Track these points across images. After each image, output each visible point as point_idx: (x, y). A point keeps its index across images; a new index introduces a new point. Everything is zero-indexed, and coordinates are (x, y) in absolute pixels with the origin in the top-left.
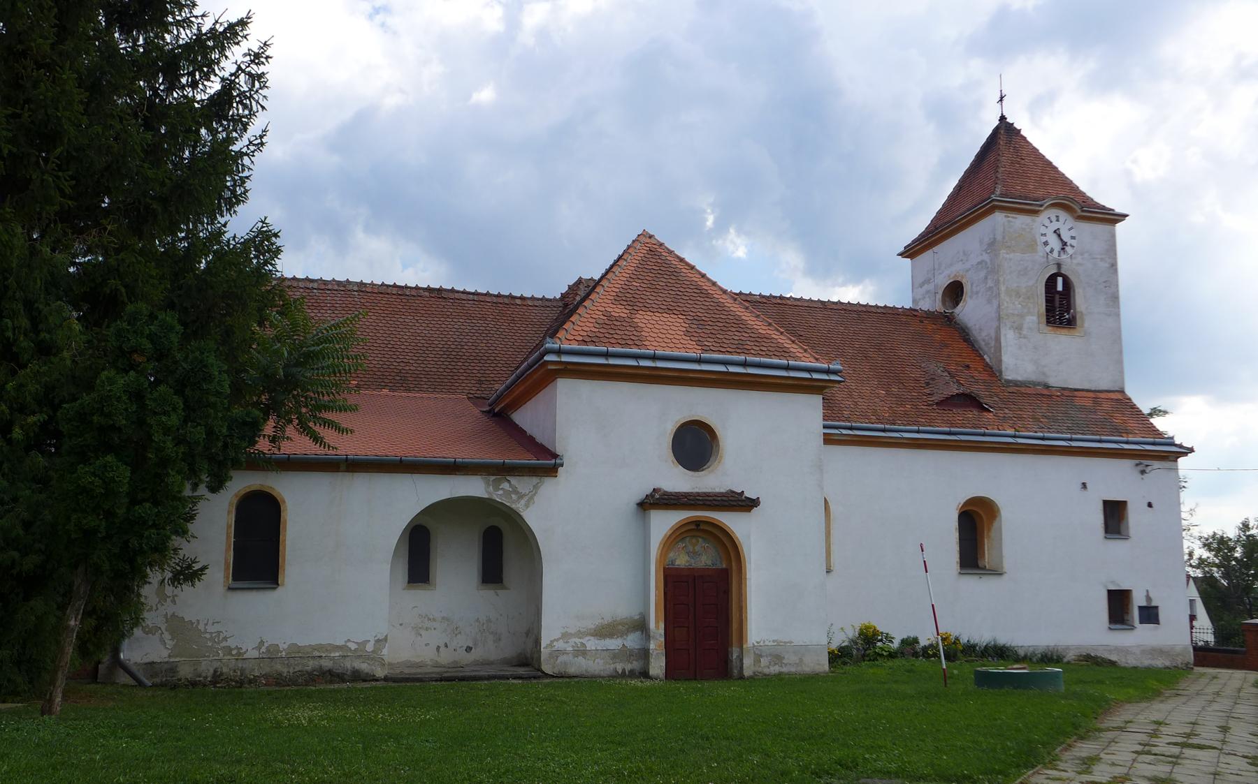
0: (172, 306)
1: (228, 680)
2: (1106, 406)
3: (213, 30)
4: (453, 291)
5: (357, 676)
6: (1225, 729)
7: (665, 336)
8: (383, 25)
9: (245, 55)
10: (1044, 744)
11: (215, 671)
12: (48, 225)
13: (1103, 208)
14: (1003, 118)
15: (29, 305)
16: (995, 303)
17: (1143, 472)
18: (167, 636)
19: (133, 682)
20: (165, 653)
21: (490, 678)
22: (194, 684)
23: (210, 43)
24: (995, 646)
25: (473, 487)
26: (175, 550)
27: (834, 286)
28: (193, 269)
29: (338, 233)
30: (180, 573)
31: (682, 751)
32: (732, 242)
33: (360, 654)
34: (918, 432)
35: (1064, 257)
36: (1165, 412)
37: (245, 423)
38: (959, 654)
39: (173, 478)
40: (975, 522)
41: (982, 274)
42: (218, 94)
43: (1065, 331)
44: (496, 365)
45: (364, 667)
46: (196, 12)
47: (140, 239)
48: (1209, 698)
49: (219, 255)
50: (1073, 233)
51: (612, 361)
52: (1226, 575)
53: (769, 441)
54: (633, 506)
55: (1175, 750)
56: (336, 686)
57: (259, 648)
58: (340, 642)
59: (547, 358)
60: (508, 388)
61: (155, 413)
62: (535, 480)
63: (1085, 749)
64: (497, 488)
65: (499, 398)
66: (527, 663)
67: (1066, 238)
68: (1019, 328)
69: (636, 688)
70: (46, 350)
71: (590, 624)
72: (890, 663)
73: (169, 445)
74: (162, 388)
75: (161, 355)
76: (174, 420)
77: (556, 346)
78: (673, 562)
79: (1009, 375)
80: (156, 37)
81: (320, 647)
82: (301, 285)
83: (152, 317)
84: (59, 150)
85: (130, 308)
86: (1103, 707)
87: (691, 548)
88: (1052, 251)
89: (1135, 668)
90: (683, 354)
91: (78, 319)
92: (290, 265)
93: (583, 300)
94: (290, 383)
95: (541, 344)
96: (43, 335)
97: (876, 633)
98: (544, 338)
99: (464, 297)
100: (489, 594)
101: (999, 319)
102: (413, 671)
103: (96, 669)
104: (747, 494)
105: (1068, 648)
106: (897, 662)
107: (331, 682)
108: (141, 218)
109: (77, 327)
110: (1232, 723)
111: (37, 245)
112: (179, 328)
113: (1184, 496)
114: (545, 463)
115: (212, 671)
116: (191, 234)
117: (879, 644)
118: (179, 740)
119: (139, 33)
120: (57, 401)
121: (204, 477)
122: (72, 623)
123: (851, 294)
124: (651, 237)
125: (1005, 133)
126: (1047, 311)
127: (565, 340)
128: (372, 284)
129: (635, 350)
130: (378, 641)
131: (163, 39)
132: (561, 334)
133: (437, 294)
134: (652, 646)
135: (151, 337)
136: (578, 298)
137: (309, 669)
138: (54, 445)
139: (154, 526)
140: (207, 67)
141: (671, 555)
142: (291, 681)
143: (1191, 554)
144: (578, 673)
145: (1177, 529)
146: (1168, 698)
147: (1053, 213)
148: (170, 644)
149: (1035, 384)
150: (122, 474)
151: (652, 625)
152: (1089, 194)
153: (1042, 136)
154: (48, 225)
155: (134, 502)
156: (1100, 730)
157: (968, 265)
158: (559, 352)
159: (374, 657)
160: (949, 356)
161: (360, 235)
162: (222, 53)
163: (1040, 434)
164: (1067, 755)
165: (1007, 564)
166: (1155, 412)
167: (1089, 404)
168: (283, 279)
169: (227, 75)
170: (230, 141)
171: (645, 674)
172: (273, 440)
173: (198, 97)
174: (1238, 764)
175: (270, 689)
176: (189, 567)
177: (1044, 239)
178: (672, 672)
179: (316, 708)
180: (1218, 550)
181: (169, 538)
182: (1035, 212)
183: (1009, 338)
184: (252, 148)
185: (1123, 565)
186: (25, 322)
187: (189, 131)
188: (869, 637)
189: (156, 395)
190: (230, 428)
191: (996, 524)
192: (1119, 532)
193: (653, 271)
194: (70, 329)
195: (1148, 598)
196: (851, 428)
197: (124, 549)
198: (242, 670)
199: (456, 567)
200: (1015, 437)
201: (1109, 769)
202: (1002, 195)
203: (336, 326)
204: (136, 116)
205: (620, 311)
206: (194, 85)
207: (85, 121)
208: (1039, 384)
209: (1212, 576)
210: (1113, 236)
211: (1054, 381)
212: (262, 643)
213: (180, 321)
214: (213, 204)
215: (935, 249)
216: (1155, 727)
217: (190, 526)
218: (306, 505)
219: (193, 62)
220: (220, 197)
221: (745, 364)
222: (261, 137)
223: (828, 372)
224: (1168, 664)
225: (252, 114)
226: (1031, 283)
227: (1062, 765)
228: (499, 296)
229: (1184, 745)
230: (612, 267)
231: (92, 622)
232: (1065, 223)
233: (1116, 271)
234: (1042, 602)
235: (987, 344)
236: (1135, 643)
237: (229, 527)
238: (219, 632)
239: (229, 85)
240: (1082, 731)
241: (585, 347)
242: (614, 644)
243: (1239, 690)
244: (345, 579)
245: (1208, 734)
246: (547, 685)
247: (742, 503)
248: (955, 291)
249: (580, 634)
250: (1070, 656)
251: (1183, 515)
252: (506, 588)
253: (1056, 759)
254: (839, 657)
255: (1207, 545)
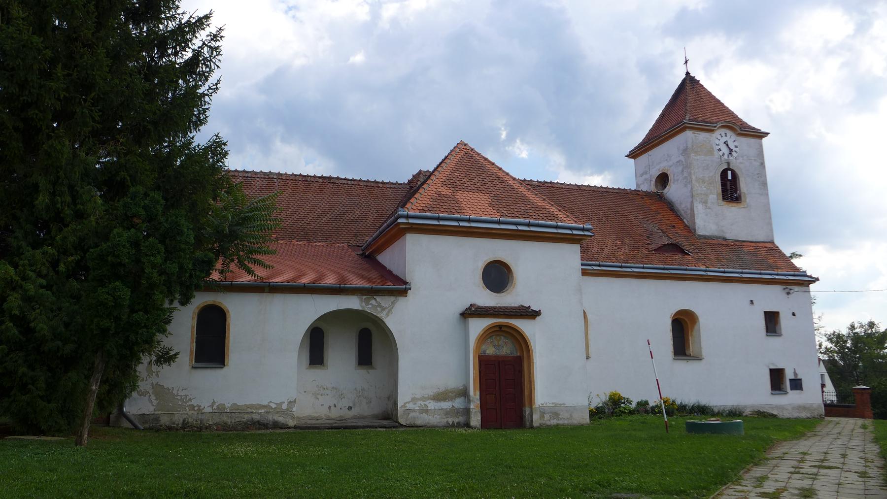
0: (158, 188)
1: (192, 426)
2: (763, 252)
3: (188, 22)
4: (338, 178)
5: (276, 425)
6: (844, 456)
7: (476, 206)
8: (294, 17)
9: (208, 36)
10: (732, 469)
11: (184, 421)
12: (84, 140)
13: (754, 128)
14: (688, 73)
15: (71, 188)
16: (689, 186)
17: (788, 293)
18: (153, 397)
19: (132, 427)
20: (152, 408)
21: (364, 427)
22: (170, 428)
23: (187, 29)
24: (699, 406)
25: (352, 303)
26: (159, 342)
27: (585, 175)
28: (172, 165)
29: (265, 143)
30: (161, 357)
31: (493, 475)
32: (518, 148)
33: (278, 411)
34: (643, 268)
35: (731, 158)
36: (800, 256)
37: (203, 262)
38: (676, 411)
39: (158, 296)
40: (683, 327)
41: (680, 168)
42: (190, 59)
43: (734, 204)
44: (362, 228)
45: (281, 419)
46: (178, 12)
47: (140, 147)
48: (835, 436)
49: (189, 157)
50: (736, 144)
51: (442, 223)
52: (842, 359)
53: (546, 274)
54: (457, 315)
55: (815, 470)
56: (263, 431)
57: (212, 406)
58: (265, 403)
59: (399, 221)
60: (374, 239)
61: (147, 255)
62: (392, 298)
63: (758, 472)
64: (367, 304)
65: (369, 245)
66: (388, 416)
67: (732, 146)
68: (705, 203)
69: (461, 434)
70: (80, 216)
71: (431, 392)
72: (630, 418)
73: (155, 275)
74: (151, 239)
75: (151, 219)
76: (159, 260)
77: (405, 213)
78: (484, 352)
79: (700, 232)
80: (154, 26)
81: (252, 406)
82: (240, 175)
83: (146, 195)
84: (93, 94)
85: (132, 189)
86: (770, 444)
87: (496, 343)
88: (723, 154)
89: (789, 419)
90: (488, 218)
91: (101, 196)
92: (233, 163)
93: (423, 184)
94: (233, 236)
95: (396, 211)
96: (79, 206)
97: (620, 398)
98: (397, 208)
99: (345, 182)
100: (363, 372)
101: (692, 196)
102: (314, 422)
103: (109, 417)
104: (533, 308)
105: (746, 407)
106: (635, 417)
107: (259, 429)
108: (141, 134)
109: (100, 201)
110: (848, 452)
111: (78, 152)
112: (163, 202)
113: (814, 308)
114: (398, 287)
115: (181, 420)
116: (172, 144)
117: (623, 405)
118: (161, 464)
119: (144, 24)
120: (86, 247)
121: (177, 296)
122: (94, 388)
123: (596, 181)
124: (466, 145)
125: (689, 83)
126: (723, 192)
127: (413, 209)
128: (286, 174)
129: (457, 216)
130: (290, 402)
131: (158, 27)
132: (408, 206)
133: (328, 180)
134: (472, 407)
135: (145, 208)
136: (419, 183)
137: (245, 420)
138: (84, 275)
139: (146, 326)
140: (184, 43)
141: (483, 347)
142: (233, 428)
143: (820, 345)
144: (423, 424)
145: (810, 330)
146: (809, 437)
147: (723, 131)
148: (155, 402)
149: (718, 238)
150: (126, 294)
151: (472, 393)
152: (745, 120)
153: (715, 84)
154: (84, 140)
155: (133, 311)
156: (768, 459)
157: (670, 163)
158: (407, 217)
159: (288, 413)
160: (661, 220)
161: (278, 144)
162: (194, 35)
163: (722, 270)
164: (747, 476)
165: (704, 353)
166: (794, 255)
167: (752, 250)
168: (229, 171)
169: (196, 48)
170: (197, 87)
171: (467, 425)
172: (222, 272)
173: (178, 61)
174: (853, 477)
175: (219, 432)
176: (167, 353)
177: (718, 147)
178: (486, 423)
179: (249, 446)
180: (837, 343)
181: (154, 334)
182: (711, 131)
183: (699, 208)
184: (211, 91)
185: (778, 353)
186: (68, 199)
187: (172, 81)
188: (615, 401)
189: (147, 243)
190: (194, 265)
191: (696, 327)
192: (775, 332)
193: (468, 166)
194: (95, 202)
195: (795, 374)
196: (599, 266)
197: (129, 341)
198: (201, 420)
199: (341, 355)
200: (706, 271)
201: (773, 483)
202: (690, 120)
203: (263, 200)
204: (140, 73)
205: (446, 191)
206: (176, 54)
207: (109, 76)
208: (720, 238)
209: (834, 359)
210: (761, 146)
211: (730, 236)
212: (214, 403)
213: (163, 197)
214: (185, 125)
215: (649, 153)
216: (802, 456)
217: (168, 327)
218: (244, 316)
219: (176, 40)
220: (190, 121)
221: (529, 225)
222: (216, 84)
223: (583, 229)
224: (809, 415)
225: (211, 71)
226: (711, 174)
227: (744, 483)
228: (368, 181)
229: (820, 467)
230: (441, 163)
231: (106, 387)
232: (731, 137)
233: (764, 167)
234: (728, 376)
235: (685, 212)
236: (788, 403)
237: (193, 327)
238: (186, 396)
239: (197, 54)
240: (756, 460)
241: (424, 214)
242: (446, 405)
243: (852, 431)
244: (267, 361)
245: (834, 459)
246: (402, 432)
247: (530, 314)
248: (663, 179)
249: (423, 399)
250: (747, 412)
251: (815, 321)
252: (373, 368)
253: (740, 478)
254: (596, 414)
255: (830, 340)
